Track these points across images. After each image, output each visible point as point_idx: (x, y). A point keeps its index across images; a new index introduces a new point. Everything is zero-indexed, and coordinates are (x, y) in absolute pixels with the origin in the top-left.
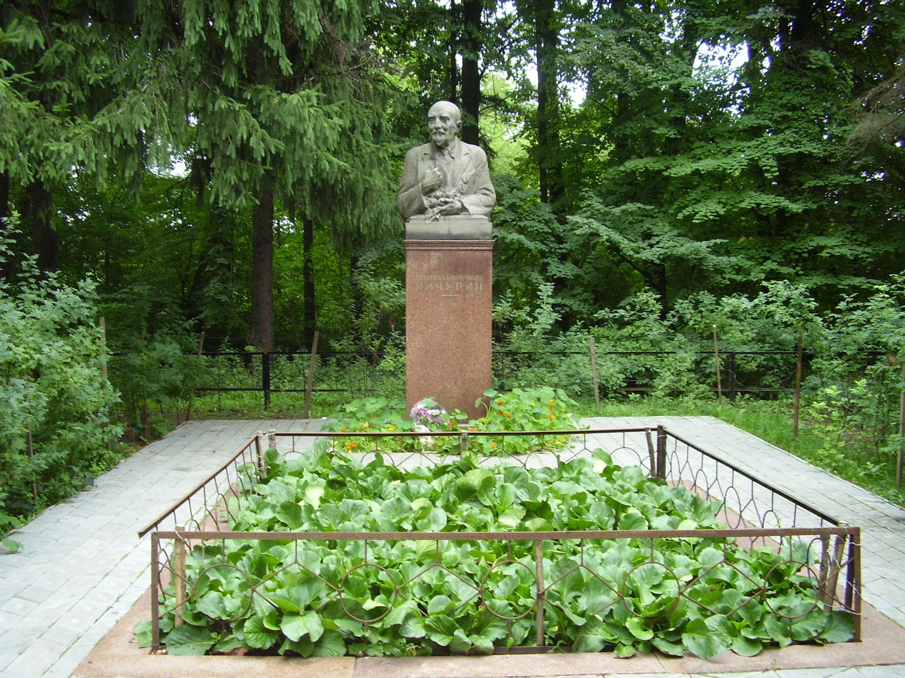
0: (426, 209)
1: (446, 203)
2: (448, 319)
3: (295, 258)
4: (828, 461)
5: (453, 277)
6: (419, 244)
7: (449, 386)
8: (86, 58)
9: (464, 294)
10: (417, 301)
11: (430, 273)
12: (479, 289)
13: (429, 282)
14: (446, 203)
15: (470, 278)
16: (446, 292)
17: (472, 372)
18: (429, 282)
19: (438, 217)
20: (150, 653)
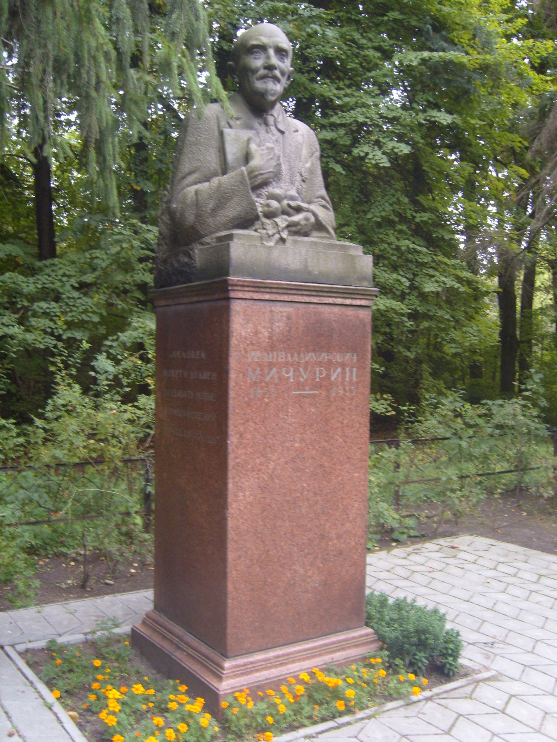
0: (257, 218)
1: (298, 210)
2: (302, 440)
3: (65, 327)
4: (442, 284)
5: (311, 357)
6: (257, 288)
7: (302, 571)
8: (197, 198)
9: (328, 390)
10: (248, 404)
11: (272, 347)
12: (351, 380)
13: (271, 365)
14: (298, 210)
15: (338, 358)
16: (300, 386)
17: (339, 537)
18: (271, 365)
19: (285, 235)
20: (426, 606)
